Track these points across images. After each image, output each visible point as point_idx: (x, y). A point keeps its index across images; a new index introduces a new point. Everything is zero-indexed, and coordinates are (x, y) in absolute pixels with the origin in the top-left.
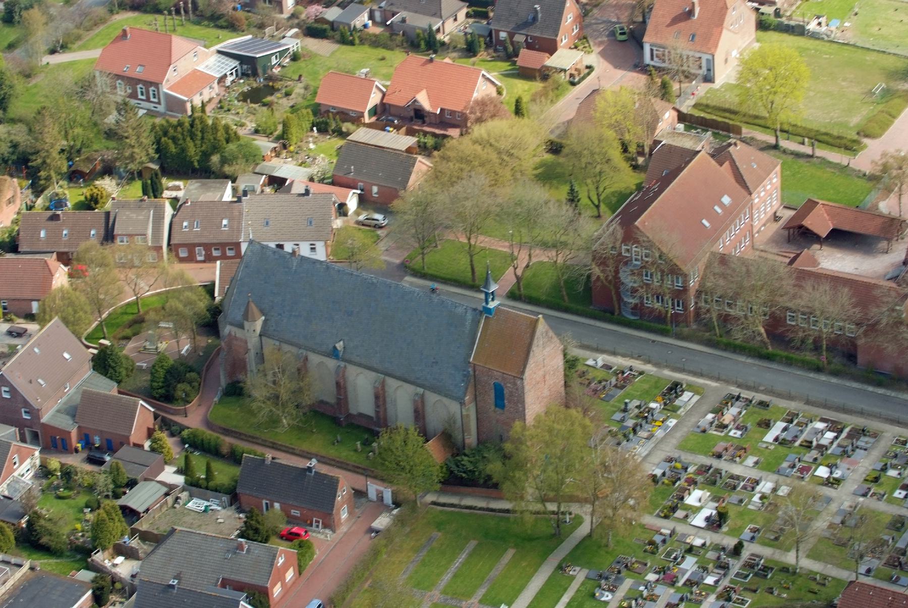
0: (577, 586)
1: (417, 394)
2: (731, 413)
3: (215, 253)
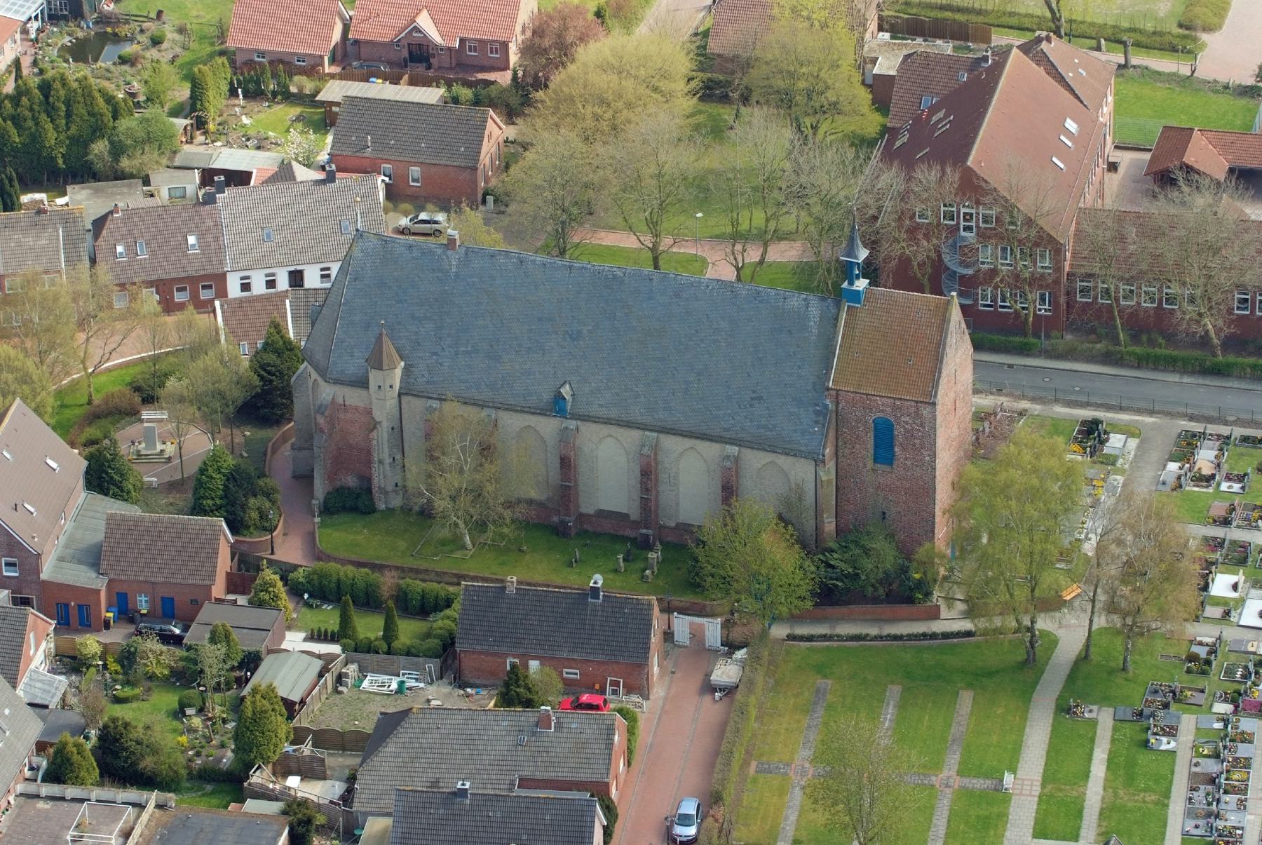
0: (1109, 733)
1: (728, 457)
2: (1205, 458)
3: (179, 297)
